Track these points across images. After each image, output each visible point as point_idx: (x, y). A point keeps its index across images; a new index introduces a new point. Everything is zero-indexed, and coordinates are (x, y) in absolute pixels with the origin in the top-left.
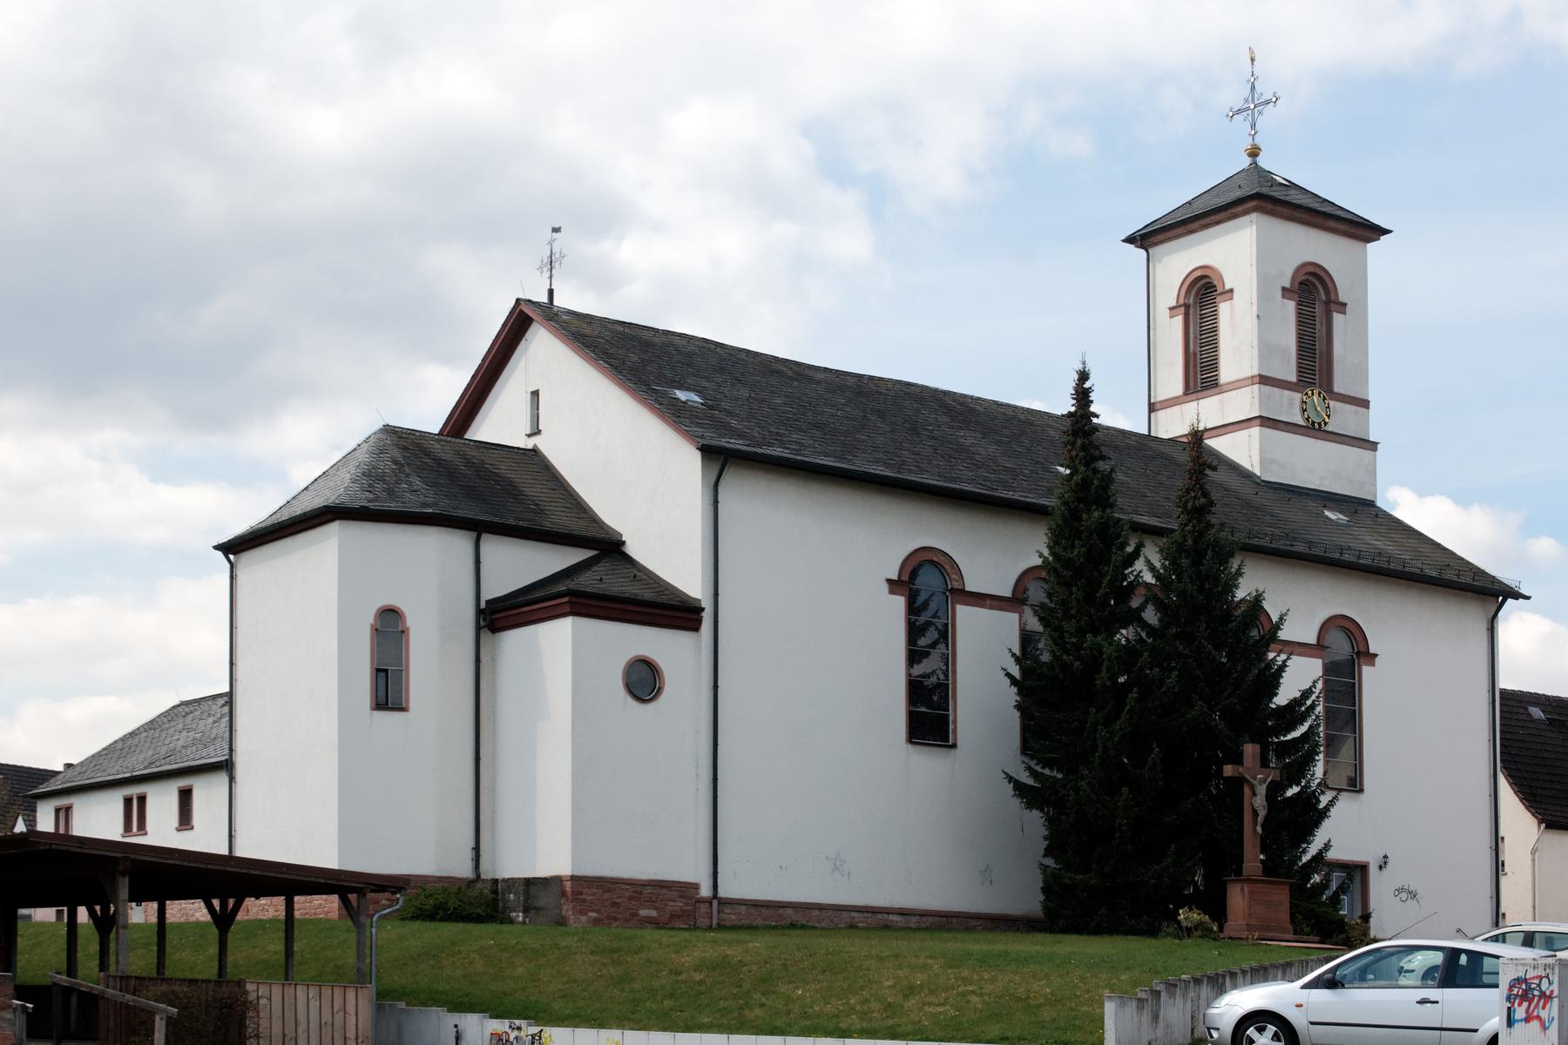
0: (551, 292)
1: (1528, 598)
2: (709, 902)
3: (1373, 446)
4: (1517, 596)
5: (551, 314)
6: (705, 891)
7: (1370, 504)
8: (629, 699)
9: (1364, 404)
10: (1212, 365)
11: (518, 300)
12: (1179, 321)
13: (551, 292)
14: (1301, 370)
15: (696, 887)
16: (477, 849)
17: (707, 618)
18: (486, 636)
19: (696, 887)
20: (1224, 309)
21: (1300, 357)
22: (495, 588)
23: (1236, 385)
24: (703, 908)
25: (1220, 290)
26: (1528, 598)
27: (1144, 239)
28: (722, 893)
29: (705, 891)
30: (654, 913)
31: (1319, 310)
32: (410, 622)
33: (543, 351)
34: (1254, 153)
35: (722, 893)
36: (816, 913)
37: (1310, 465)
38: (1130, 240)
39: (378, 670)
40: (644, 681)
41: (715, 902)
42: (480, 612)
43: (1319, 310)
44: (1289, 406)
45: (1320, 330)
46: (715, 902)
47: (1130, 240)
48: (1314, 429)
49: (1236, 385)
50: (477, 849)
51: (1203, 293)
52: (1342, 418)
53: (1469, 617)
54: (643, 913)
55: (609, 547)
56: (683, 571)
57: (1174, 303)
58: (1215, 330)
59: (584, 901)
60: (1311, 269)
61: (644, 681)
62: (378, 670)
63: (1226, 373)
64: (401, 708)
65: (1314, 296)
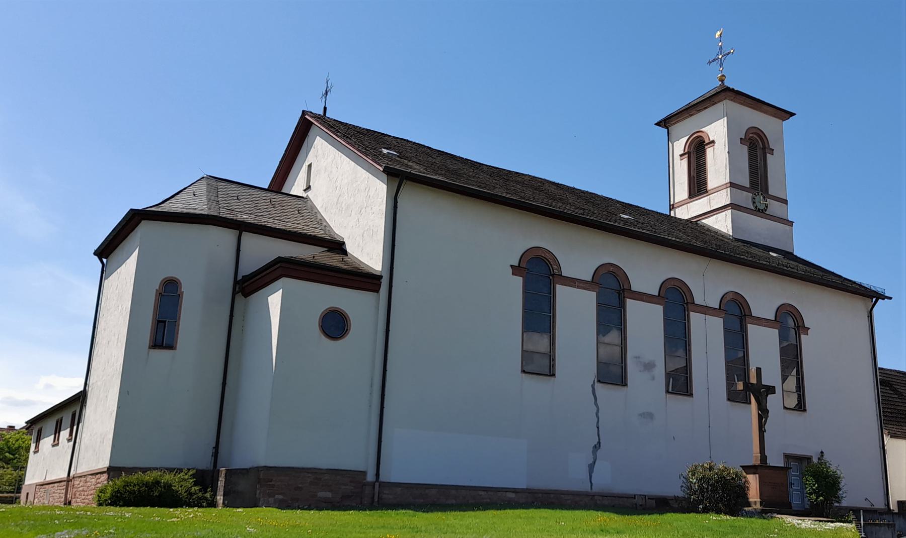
0: (325, 109)
1: (890, 298)
2: (373, 485)
3: (791, 224)
4: (883, 297)
5: (323, 119)
6: (370, 477)
7: (792, 254)
8: (323, 337)
9: (785, 202)
10: (705, 183)
11: (304, 113)
12: (685, 162)
13: (325, 109)
14: (751, 183)
15: (364, 473)
16: (217, 448)
17: (385, 282)
18: (239, 298)
19: (364, 473)
20: (709, 151)
21: (750, 172)
22: (247, 269)
23: (717, 190)
24: (368, 490)
25: (707, 141)
26: (890, 298)
27: (665, 123)
28: (383, 478)
29: (370, 477)
30: (329, 495)
31: (759, 152)
32: (185, 288)
33: (322, 153)
34: (722, 81)
35: (383, 478)
36: (453, 492)
37: (760, 230)
38: (658, 124)
39: (159, 322)
40: (335, 325)
41: (377, 484)
42: (236, 282)
43: (759, 152)
44: (745, 198)
45: (760, 163)
46: (377, 484)
47: (658, 124)
48: (761, 212)
49: (717, 190)
50: (217, 448)
51: (697, 150)
52: (774, 207)
53: (859, 305)
54: (321, 494)
55: (337, 247)
56: (368, 252)
57: (682, 152)
58: (705, 164)
59: (273, 486)
60: (755, 131)
61: (335, 325)
62: (159, 322)
63: (711, 184)
64: (171, 347)
65: (756, 149)
